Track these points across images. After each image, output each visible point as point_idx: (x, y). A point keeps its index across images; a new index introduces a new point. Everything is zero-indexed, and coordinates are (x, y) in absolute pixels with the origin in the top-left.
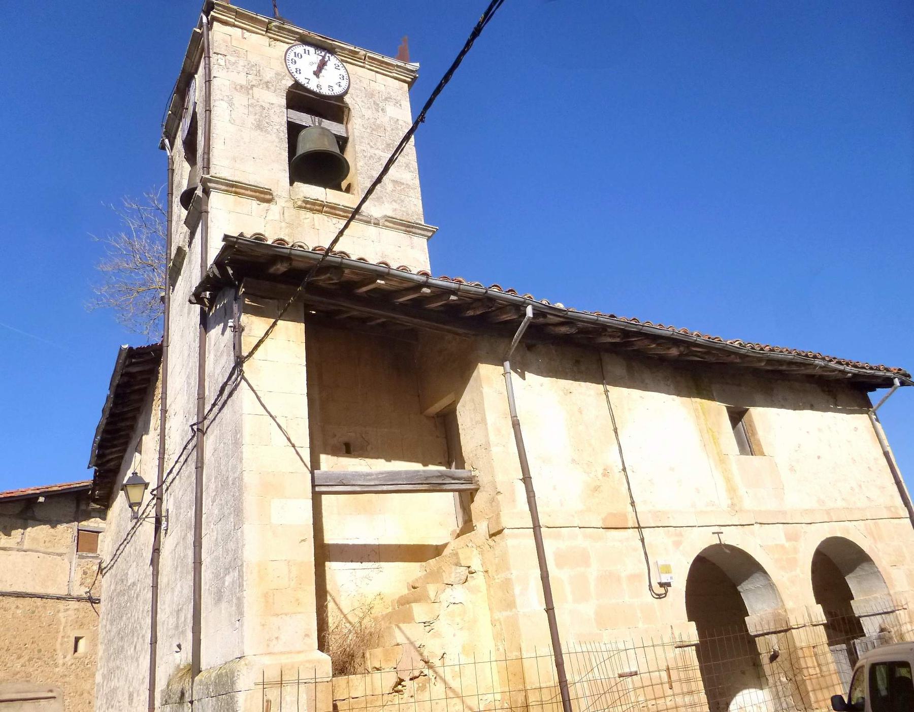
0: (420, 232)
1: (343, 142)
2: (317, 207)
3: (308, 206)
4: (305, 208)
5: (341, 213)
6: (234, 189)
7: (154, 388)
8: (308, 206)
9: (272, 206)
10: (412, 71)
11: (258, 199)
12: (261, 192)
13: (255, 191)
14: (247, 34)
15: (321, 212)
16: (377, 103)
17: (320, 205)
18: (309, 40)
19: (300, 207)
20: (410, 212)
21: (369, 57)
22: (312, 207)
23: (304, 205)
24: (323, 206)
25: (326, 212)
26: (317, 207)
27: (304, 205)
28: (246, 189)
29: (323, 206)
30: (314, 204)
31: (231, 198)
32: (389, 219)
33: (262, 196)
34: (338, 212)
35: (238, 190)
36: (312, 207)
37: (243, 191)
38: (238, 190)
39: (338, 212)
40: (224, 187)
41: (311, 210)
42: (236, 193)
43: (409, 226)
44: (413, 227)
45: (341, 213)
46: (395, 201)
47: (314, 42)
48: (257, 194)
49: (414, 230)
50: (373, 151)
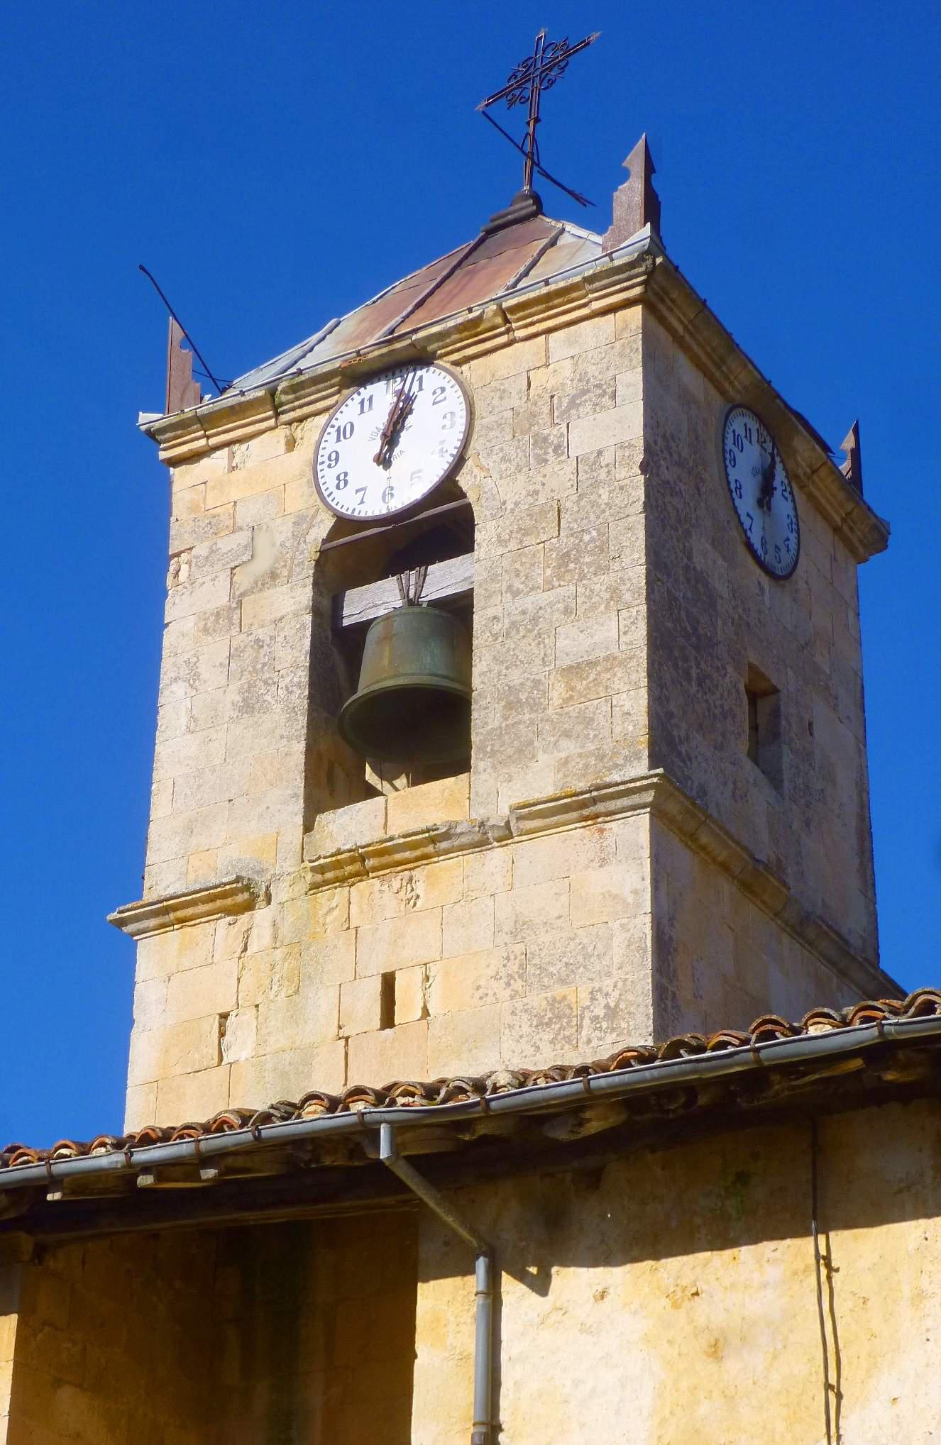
0: (620, 803)
1: (456, 614)
2: (349, 869)
3: (329, 875)
4: (326, 883)
5: (408, 855)
6: (172, 916)
7: (534, 1102)
8: (329, 875)
9: (262, 916)
10: (631, 265)
11: (229, 911)
12: (224, 895)
13: (212, 899)
14: (239, 449)
15: (363, 874)
16: (539, 437)
17: (352, 861)
18: (365, 368)
19: (315, 886)
20: (607, 748)
21: (514, 309)
22: (339, 873)
23: (319, 878)
24: (363, 858)
25: (375, 869)
26: (349, 869)
27: (319, 878)
28: (193, 903)
29: (363, 858)
30: (338, 865)
31: (174, 937)
32: (525, 811)
33: (229, 901)
34: (398, 857)
35: (180, 914)
36: (339, 873)
37: (189, 911)
38: (180, 914)
39: (398, 857)
40: (153, 922)
41: (342, 880)
42: (181, 921)
43: (583, 805)
44: (594, 801)
45: (408, 855)
46: (567, 734)
47: (378, 365)
48: (219, 903)
49: (600, 807)
50: (528, 602)
